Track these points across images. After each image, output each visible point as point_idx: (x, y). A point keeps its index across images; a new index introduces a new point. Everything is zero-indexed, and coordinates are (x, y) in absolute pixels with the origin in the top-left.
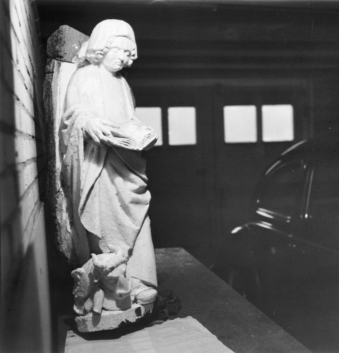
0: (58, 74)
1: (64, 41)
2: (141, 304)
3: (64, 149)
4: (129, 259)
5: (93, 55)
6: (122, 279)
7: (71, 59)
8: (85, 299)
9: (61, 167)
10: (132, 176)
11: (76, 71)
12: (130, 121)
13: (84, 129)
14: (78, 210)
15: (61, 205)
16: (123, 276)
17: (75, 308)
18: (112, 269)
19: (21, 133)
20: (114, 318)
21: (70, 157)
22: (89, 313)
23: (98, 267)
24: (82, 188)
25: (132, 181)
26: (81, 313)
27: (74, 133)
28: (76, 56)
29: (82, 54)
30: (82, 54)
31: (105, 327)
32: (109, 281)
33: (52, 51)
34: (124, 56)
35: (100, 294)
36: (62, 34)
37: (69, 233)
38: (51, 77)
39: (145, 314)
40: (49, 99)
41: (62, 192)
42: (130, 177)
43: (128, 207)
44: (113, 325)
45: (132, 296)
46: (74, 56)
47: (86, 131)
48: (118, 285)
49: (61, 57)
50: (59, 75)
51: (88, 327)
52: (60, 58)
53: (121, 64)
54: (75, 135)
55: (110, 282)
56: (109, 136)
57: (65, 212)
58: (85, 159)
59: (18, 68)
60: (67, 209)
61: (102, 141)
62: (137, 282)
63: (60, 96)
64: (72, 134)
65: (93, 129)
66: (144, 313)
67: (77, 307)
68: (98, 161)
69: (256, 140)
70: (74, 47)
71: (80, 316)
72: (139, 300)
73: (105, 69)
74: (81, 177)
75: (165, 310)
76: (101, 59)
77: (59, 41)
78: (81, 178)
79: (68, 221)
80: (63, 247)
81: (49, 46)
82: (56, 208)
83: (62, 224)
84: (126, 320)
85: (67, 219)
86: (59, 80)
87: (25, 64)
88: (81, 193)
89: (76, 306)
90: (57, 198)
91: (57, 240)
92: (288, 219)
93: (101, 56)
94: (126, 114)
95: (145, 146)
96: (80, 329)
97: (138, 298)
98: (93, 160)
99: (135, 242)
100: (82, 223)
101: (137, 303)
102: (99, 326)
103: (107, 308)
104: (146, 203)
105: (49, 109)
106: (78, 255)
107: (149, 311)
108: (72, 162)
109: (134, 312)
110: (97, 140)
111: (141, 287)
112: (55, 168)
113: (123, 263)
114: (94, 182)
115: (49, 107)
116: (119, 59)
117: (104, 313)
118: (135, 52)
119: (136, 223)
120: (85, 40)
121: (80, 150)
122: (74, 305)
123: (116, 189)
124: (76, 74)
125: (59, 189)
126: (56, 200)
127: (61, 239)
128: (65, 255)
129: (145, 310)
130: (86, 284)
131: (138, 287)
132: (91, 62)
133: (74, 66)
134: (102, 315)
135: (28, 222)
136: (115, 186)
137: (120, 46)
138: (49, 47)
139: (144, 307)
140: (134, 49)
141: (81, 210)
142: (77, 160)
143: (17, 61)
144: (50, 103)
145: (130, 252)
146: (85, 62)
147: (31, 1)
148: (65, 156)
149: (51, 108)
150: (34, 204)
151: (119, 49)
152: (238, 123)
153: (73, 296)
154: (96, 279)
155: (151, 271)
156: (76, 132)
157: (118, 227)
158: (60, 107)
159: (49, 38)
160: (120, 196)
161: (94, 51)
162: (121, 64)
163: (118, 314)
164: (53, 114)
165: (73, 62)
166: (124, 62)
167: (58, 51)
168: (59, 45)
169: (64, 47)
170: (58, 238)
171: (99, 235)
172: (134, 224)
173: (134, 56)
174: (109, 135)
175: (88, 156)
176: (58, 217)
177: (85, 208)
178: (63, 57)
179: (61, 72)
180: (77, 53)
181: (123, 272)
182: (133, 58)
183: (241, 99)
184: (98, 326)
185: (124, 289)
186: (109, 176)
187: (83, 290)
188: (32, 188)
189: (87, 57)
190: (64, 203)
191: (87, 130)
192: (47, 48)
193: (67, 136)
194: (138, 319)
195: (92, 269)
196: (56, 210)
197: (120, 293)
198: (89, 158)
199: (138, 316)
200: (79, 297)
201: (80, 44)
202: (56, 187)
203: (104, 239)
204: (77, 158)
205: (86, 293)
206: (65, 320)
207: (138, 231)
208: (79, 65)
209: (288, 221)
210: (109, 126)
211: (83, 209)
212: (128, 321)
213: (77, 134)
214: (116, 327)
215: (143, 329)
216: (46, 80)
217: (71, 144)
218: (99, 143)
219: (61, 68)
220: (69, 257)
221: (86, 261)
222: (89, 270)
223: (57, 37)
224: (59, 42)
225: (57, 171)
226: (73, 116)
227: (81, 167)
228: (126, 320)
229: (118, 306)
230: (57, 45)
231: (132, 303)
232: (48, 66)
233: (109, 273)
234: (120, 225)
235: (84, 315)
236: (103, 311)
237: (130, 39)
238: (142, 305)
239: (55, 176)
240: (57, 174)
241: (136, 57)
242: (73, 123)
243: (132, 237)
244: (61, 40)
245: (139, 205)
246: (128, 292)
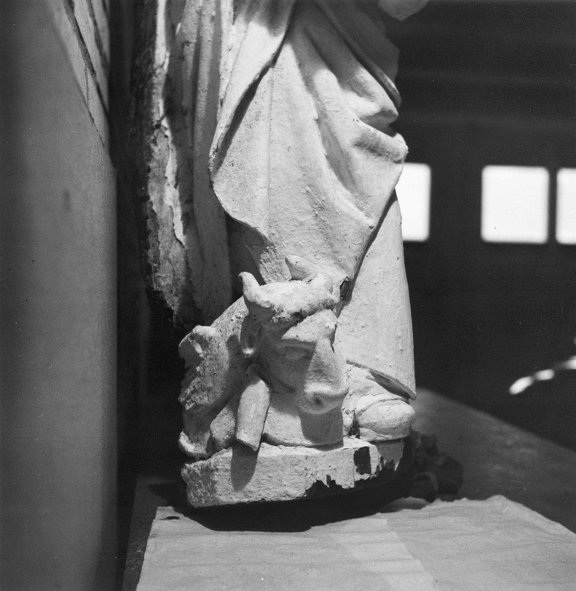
2: (371, 439)
4: (342, 311)
6: (323, 352)
8: (214, 411)
9: (167, 61)
14: (209, 153)
15: (162, 165)
16: (327, 342)
17: (184, 440)
18: (299, 316)
20: (296, 468)
21: (195, 15)
22: (224, 450)
23: (259, 306)
24: (222, 97)
25: (362, 91)
26: (201, 450)
31: (268, 491)
32: (287, 356)
35: (257, 394)
37: (178, 244)
39: (381, 469)
41: (166, 129)
42: (357, 76)
43: (347, 158)
44: (294, 488)
45: (348, 414)
48: (310, 368)
51: (219, 488)
55: (289, 357)
57: (172, 186)
58: (234, 19)
60: (177, 179)
62: (360, 376)
66: (378, 467)
67: (190, 439)
68: (272, 23)
71: (196, 461)
72: (366, 426)
74: (222, 62)
75: (429, 474)
78: (222, 67)
79: (178, 211)
80: (160, 280)
82: (149, 170)
83: (162, 216)
84: (328, 477)
85: (176, 205)
88: (219, 111)
89: (187, 434)
90: (152, 145)
91: (146, 257)
96: (195, 495)
97: (362, 421)
98: (258, 14)
99: (360, 261)
100: (217, 195)
101: (358, 437)
102: (249, 487)
103: (277, 437)
104: (396, 159)
106: (199, 305)
107: (392, 463)
109: (352, 460)
111: (372, 391)
113: (328, 307)
114: (258, 76)
117: (267, 452)
119: (367, 207)
122: (182, 433)
123: (317, 106)
126: (149, 148)
127: (157, 256)
128: (166, 302)
129: (382, 459)
130: (220, 367)
131: (363, 392)
134: (261, 454)
136: (316, 96)
139: (378, 449)
141: (216, 151)
142: (213, 19)
145: (347, 289)
153: (181, 407)
154: (251, 346)
155: (400, 348)
157: (316, 215)
160: (326, 124)
163: (307, 457)
170: (150, 253)
171: (264, 231)
172: (361, 209)
175: (245, 8)
176: (153, 197)
177: (228, 152)
181: (329, 333)
184: (247, 486)
185: (330, 382)
186: (301, 65)
187: (210, 384)
190: (170, 160)
194: (361, 480)
195: (237, 325)
196: (149, 178)
197: (315, 394)
199: (362, 474)
200: (197, 406)
203: (275, 251)
204: (214, 13)
205: (219, 392)
206: (151, 458)
207: (372, 230)
211: (222, 151)
212: (334, 481)
214: (298, 495)
215: (374, 515)
220: (175, 308)
221: (220, 312)
222: (231, 327)
225: (158, 71)
227: (223, 35)
228: (328, 477)
229: (307, 434)
231: (345, 433)
233: (287, 329)
234: (321, 208)
235: (210, 457)
236: (264, 444)
238: (373, 442)
239: (152, 86)
240: (155, 80)
243: (355, 247)
245: (379, 158)
246: (339, 391)
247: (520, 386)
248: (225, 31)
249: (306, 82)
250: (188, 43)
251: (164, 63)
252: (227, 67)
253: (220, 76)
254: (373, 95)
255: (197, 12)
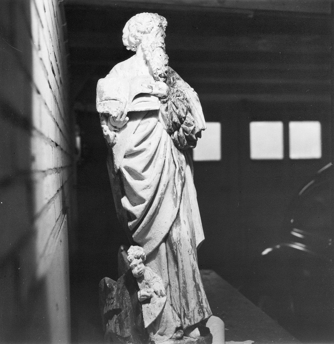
19: (41, 134)
59: (40, 56)
69: (282, 157)
87: (50, 60)
92: (329, 242)
135: (47, 243)
143: (39, 46)
147: (59, 1)
150: (55, 221)
152: (265, 139)
183: (267, 115)
188: (53, 202)
209: (330, 244)
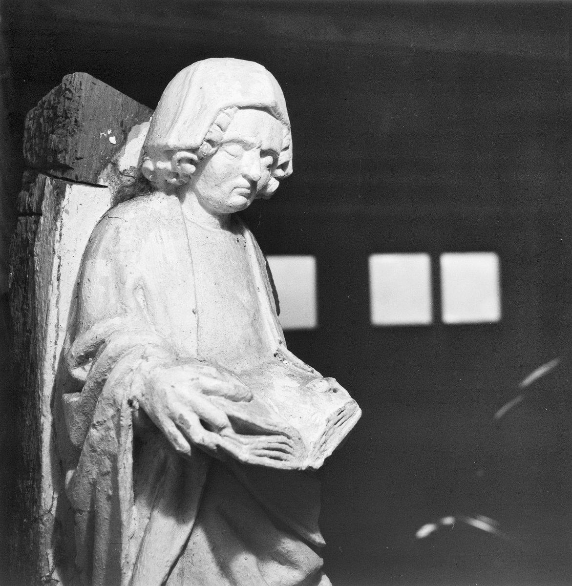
0: (56, 220)
1: (76, 121)
3: (68, 455)
5: (165, 165)
7: (97, 174)
10: (285, 546)
11: (108, 211)
12: (273, 363)
13: (136, 404)
21: (88, 486)
25: (285, 560)
27: (104, 413)
28: (110, 166)
29: (129, 158)
30: (129, 158)
33: (37, 149)
34: (256, 167)
36: (68, 99)
38: (33, 226)
40: (26, 291)
42: (280, 548)
46: (105, 166)
47: (141, 410)
49: (66, 168)
50: (58, 224)
52: (66, 175)
53: (248, 191)
54: (105, 421)
56: (224, 432)
61: (198, 449)
63: (58, 285)
64: (97, 418)
65: (168, 408)
70: (107, 139)
73: (201, 208)
76: (188, 176)
77: (60, 119)
81: (29, 136)
86: (57, 237)
93: (191, 168)
94: (260, 340)
95: (329, 453)
105: (25, 323)
108: (94, 501)
110: (183, 445)
112: (39, 507)
115: (25, 316)
116: (245, 176)
118: (286, 156)
120: (139, 119)
121: (121, 471)
124: (113, 221)
125: (48, 574)
132: (158, 186)
133: (102, 197)
137: (250, 139)
138: (30, 139)
140: (287, 148)
142: (109, 498)
144: (28, 305)
146: (140, 184)
148: (70, 474)
149: (29, 321)
151: (246, 146)
156: (111, 412)
158: (58, 320)
159: (31, 111)
161: (169, 153)
162: (248, 191)
164: (36, 338)
165: (101, 183)
166: (260, 184)
167: (56, 152)
168: (60, 131)
169: (77, 137)
173: (284, 166)
174: (224, 428)
178: (72, 169)
179: (64, 215)
180: (115, 158)
182: (280, 173)
189: (147, 169)
191: (148, 409)
192: (25, 139)
193: (78, 419)
198: (152, 494)
201: (124, 131)
202: (40, 568)
208: (118, 192)
210: (222, 396)
213: (113, 417)
216: (16, 234)
217: (91, 446)
218: (190, 454)
219: (64, 203)
223: (55, 108)
224: (59, 122)
226: (102, 358)
230: (52, 132)
232: (23, 194)
237: (278, 117)
239: (38, 534)
241: (290, 170)
242: (99, 380)
244: (67, 117)
247: (426, 530)
248: (125, 523)
249: (221, 566)
250: (81, 511)
251: (51, 508)
252: (128, 560)
253: (121, 570)
254: (296, 564)
255: (90, 483)
